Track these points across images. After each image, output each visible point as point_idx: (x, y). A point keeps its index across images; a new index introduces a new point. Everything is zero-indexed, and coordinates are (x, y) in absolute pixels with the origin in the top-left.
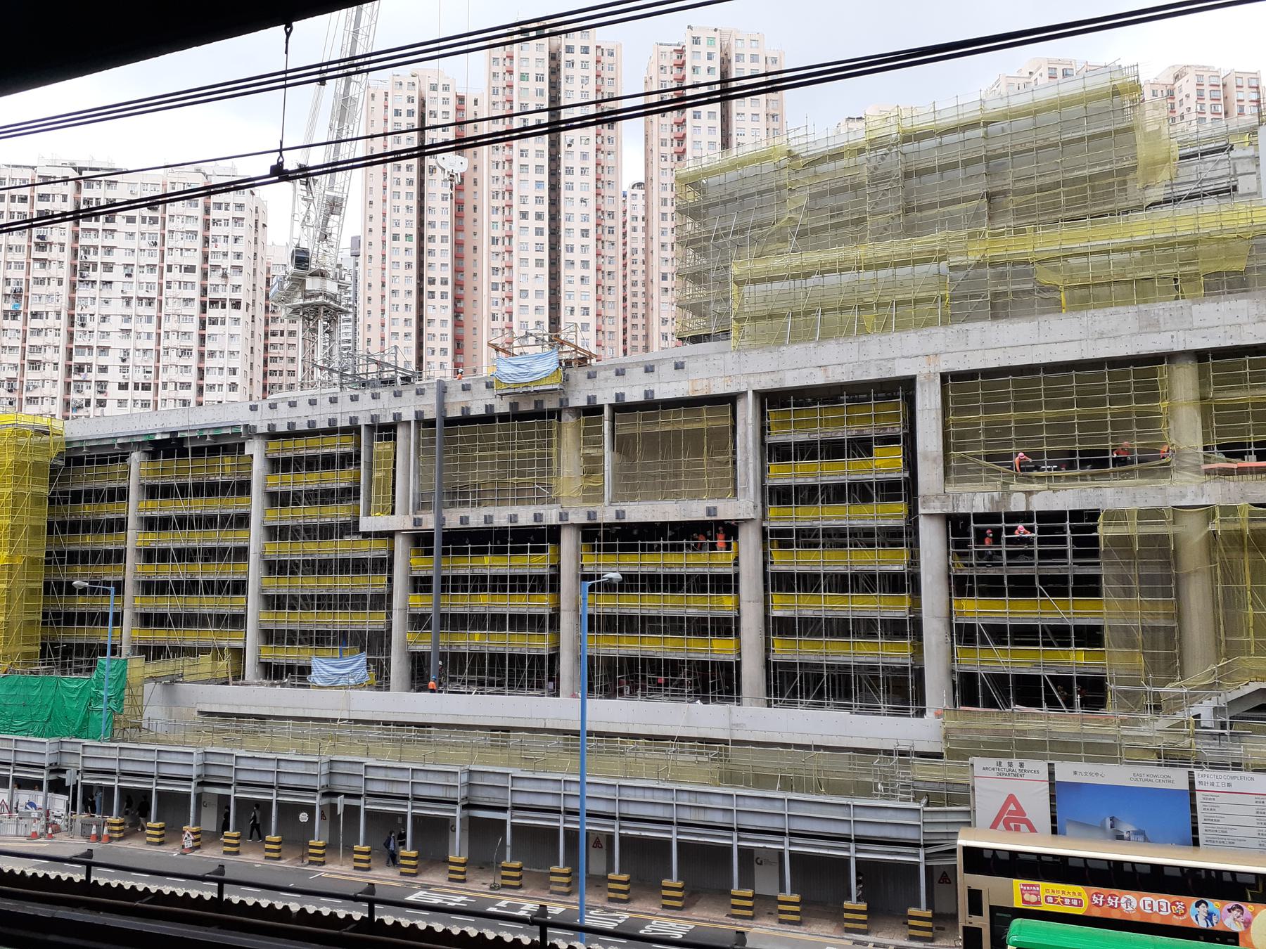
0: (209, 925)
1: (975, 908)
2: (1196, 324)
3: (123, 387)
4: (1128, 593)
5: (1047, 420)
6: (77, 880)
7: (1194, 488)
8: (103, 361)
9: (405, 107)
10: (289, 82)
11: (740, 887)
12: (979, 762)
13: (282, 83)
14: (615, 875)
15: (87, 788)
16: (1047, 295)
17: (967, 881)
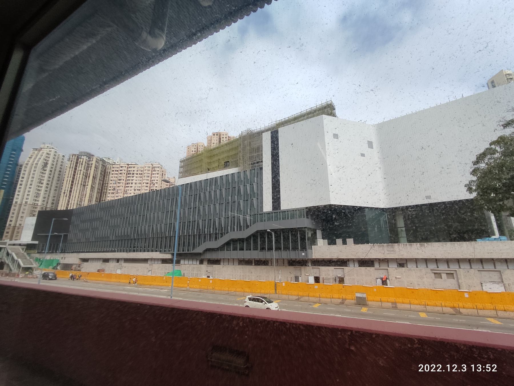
3: (137, 174)
9: (194, 150)
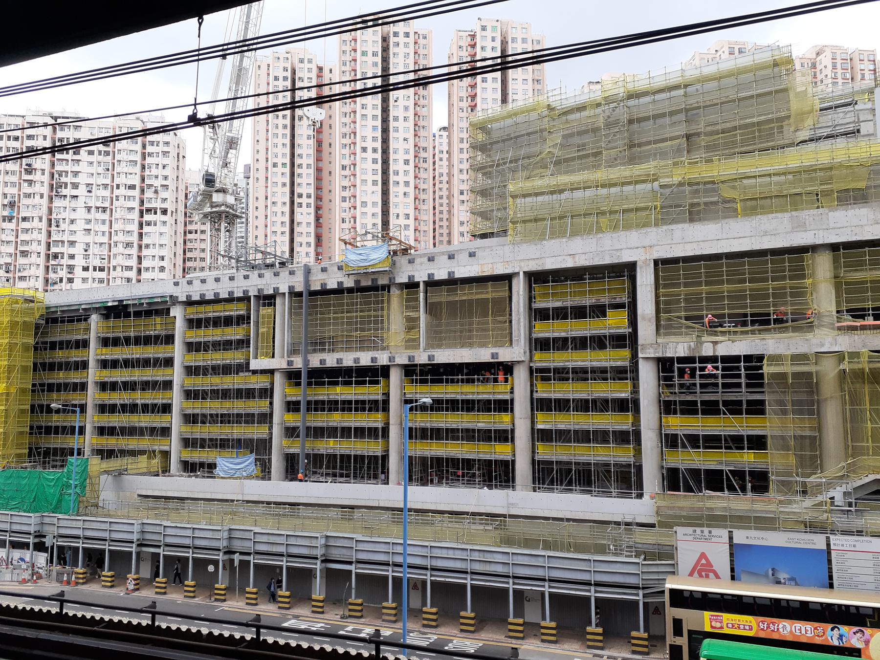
0: (145, 644)
1: (678, 631)
2: (831, 225)
3: (86, 269)
4: (784, 412)
5: (728, 292)
6: (53, 612)
7: (830, 339)
8: (72, 251)
9: (281, 74)
10: (201, 57)
11: (515, 617)
12: (680, 530)
13: (196, 58)
14: (427, 609)
15: (61, 548)
16: (728, 205)
17: (672, 613)
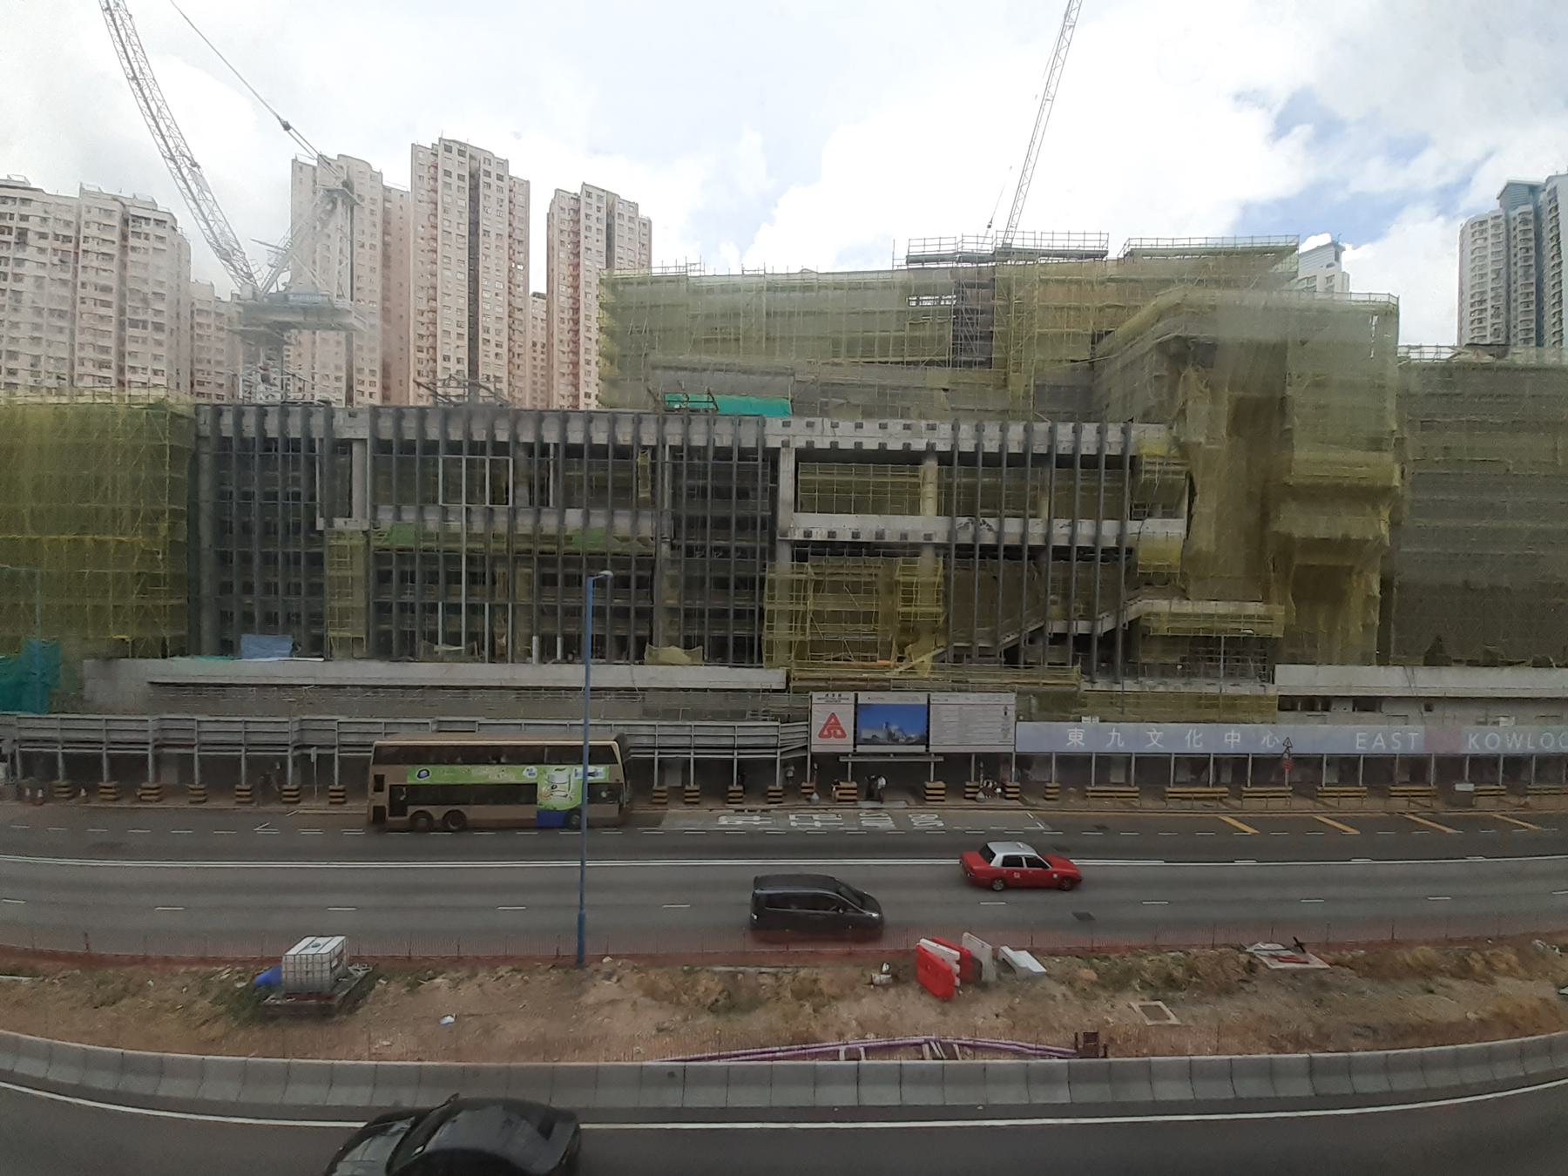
1: (379, 787)
12: (815, 695)
14: (692, 786)
15: (26, 757)
17: (374, 770)
